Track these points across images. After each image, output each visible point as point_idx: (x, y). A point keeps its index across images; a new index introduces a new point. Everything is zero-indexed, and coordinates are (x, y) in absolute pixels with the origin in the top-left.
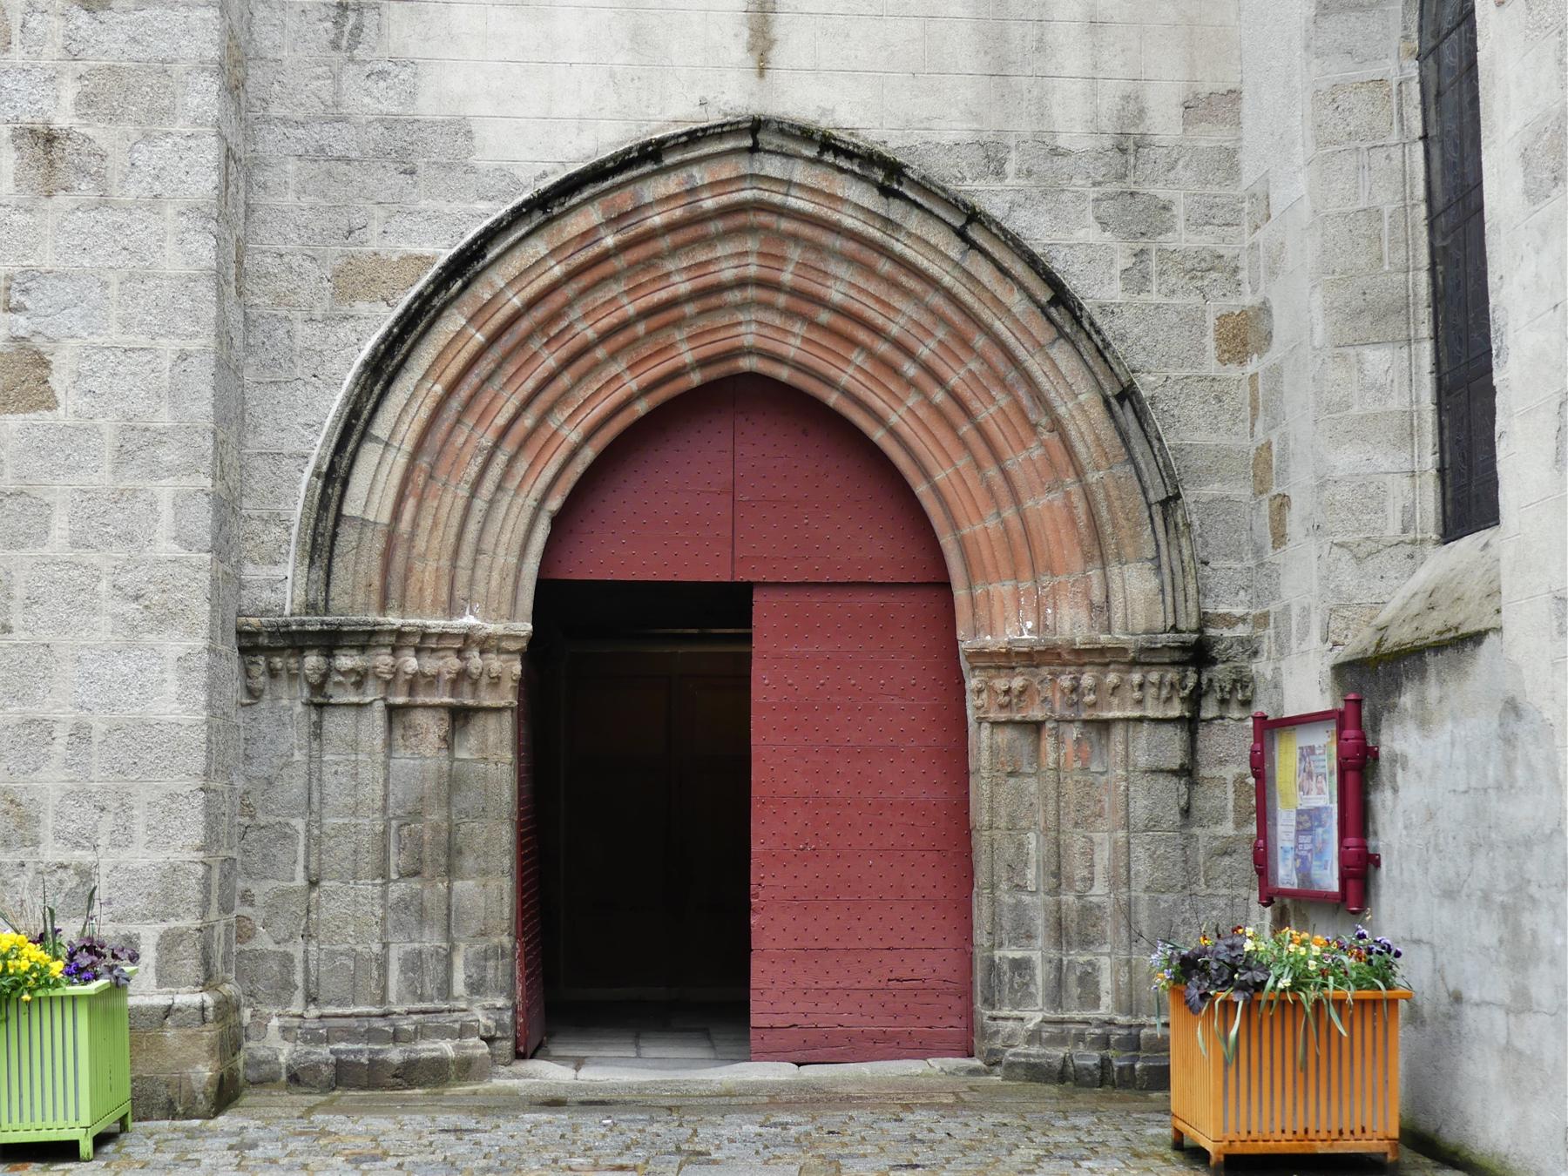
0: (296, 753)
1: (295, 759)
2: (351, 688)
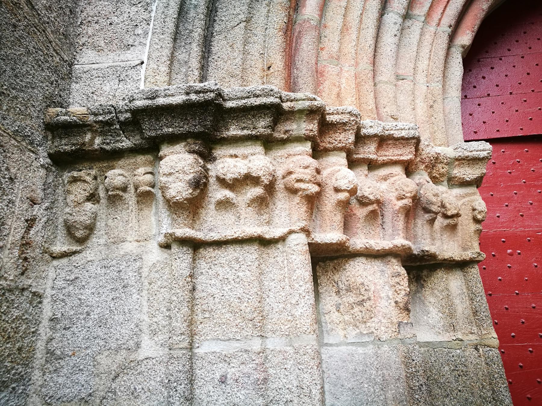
0: (146, 341)
1: (142, 354)
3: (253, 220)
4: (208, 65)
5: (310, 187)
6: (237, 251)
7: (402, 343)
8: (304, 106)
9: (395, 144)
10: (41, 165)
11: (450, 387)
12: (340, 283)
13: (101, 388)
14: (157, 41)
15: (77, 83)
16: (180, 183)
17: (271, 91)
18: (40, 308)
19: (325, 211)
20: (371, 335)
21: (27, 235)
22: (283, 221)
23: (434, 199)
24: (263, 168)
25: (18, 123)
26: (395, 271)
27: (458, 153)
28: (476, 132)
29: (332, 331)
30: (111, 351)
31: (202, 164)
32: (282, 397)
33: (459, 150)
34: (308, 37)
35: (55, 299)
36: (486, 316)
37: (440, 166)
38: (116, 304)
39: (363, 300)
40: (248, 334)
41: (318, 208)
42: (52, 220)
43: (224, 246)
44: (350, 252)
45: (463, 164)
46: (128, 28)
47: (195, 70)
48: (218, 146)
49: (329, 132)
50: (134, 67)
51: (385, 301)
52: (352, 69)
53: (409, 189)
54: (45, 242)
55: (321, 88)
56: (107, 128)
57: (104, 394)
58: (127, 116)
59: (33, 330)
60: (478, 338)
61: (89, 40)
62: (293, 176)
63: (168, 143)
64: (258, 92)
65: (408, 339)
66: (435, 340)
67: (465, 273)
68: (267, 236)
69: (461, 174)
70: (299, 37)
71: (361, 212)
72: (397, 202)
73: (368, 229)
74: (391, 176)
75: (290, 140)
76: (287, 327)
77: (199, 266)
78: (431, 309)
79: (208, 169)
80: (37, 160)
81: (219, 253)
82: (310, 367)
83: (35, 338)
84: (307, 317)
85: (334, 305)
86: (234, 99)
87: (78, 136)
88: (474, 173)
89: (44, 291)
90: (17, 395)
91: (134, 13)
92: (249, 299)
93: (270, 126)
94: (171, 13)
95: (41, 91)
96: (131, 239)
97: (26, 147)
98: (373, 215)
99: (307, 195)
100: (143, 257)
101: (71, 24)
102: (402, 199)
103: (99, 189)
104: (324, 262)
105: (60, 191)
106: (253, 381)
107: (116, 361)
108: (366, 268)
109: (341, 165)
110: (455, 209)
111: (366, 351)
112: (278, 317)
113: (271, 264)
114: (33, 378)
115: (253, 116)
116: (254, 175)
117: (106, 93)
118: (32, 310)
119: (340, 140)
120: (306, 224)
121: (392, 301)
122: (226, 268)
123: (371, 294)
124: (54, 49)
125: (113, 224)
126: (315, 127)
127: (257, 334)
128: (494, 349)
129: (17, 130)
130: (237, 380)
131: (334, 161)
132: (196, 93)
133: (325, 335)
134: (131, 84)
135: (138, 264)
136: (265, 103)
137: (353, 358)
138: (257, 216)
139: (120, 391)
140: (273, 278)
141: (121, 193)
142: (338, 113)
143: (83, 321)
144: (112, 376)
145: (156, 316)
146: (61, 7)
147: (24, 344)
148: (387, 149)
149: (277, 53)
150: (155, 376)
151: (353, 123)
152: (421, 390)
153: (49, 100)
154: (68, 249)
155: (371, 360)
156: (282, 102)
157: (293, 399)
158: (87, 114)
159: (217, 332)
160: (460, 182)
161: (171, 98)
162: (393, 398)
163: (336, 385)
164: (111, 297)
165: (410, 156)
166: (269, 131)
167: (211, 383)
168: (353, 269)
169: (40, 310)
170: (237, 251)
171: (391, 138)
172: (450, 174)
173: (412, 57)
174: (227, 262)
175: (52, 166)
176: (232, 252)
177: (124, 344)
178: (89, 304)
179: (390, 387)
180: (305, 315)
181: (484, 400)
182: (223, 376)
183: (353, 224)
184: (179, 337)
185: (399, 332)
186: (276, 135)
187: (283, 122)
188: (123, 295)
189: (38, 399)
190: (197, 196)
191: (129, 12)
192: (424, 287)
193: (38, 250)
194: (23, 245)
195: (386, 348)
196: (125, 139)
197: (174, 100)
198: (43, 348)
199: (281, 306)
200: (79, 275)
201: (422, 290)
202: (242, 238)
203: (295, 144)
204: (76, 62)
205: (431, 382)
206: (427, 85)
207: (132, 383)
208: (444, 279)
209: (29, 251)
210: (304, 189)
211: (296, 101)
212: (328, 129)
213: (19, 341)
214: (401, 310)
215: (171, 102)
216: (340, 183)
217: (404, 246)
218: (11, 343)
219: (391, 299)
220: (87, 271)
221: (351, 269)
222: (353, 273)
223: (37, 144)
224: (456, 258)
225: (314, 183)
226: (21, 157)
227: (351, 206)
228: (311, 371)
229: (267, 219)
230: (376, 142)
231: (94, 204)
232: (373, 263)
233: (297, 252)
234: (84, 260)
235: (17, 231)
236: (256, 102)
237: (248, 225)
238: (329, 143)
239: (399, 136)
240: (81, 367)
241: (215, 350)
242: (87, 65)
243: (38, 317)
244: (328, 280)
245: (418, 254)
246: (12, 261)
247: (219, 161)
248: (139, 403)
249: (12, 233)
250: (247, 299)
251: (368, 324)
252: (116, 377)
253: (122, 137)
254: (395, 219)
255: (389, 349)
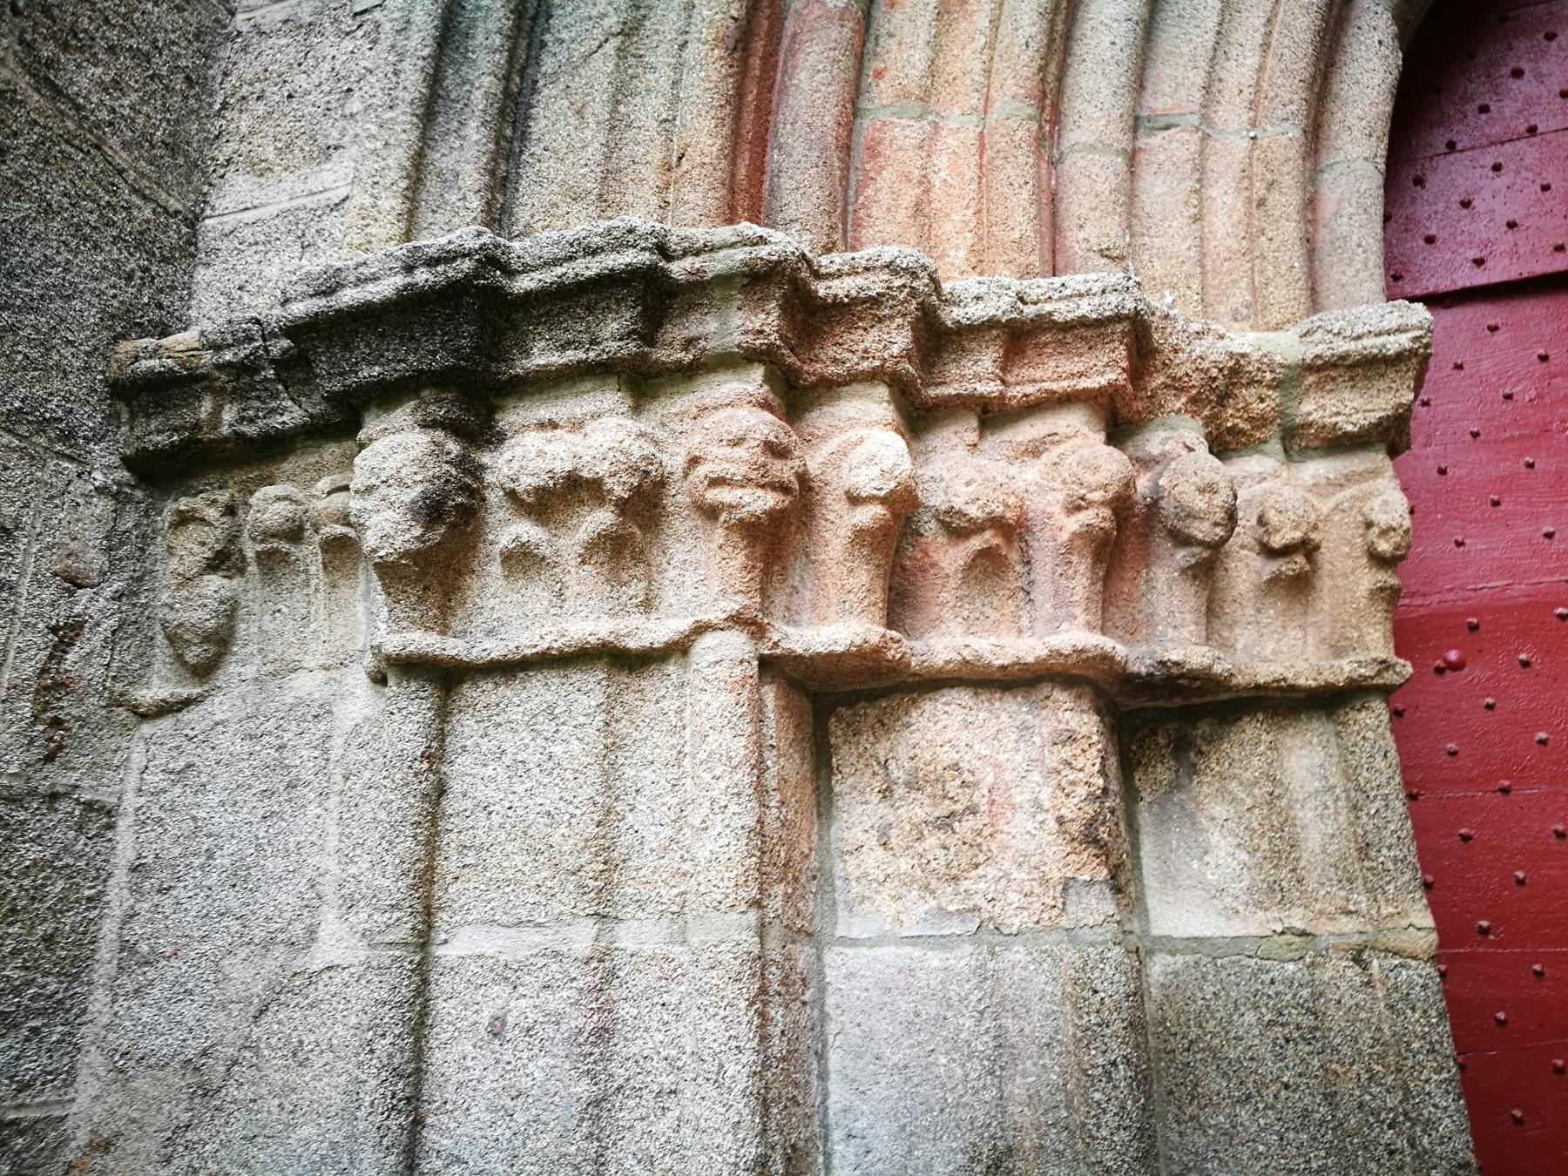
0: (331, 925)
1: (318, 958)
2: (583, 580)
3: (596, 601)
4: (518, 174)
5: (747, 499)
6: (553, 688)
7: (1070, 941)
8: (731, 264)
9: (1062, 344)
10: (97, 489)
11: (1256, 1073)
12: (892, 765)
13: (229, 1037)
14: (374, 129)
15: (207, 265)
16: (390, 514)
17: (631, 231)
18: (110, 840)
19: (824, 561)
20: (970, 915)
21: (59, 663)
22: (690, 597)
23: (1199, 503)
24: (611, 454)
25: (22, 391)
26: (1062, 726)
27: (1311, 346)
28: (1479, 262)
29: (862, 902)
30: (252, 947)
31: (453, 456)
32: (649, 1079)
33: (1318, 336)
34: (816, 49)
35: (143, 817)
36: (1395, 860)
37: (1250, 394)
38: (271, 831)
39: (952, 814)
40: (563, 908)
41: (807, 555)
42: (135, 622)
43: (521, 675)
44: (915, 674)
45: (1334, 379)
46: (329, 102)
47: (471, 196)
48: (511, 400)
49: (832, 328)
50: (336, 205)
51: (1025, 816)
52: (970, 122)
53: (1101, 477)
54: (114, 678)
55: (869, 192)
56: (247, 379)
57: (236, 1054)
58: (286, 345)
59: (87, 893)
60: (1369, 928)
61: (244, 148)
62: (702, 470)
63: (379, 406)
64: (596, 241)
65: (1086, 929)
66: (1218, 933)
67: (1340, 728)
68: (632, 644)
69: (1327, 413)
70: (792, 53)
71: (951, 557)
72: (1066, 520)
73: (978, 604)
74: (1053, 443)
75: (705, 364)
76: (675, 891)
77: (460, 729)
78: (1215, 838)
79: (483, 467)
80: (85, 477)
81: (508, 693)
82: (726, 1001)
83: (97, 912)
84: (729, 864)
85: (872, 827)
86: (534, 268)
87: (184, 407)
88: (1370, 407)
89: (119, 799)
90: (45, 1046)
91: (345, 58)
92: (573, 816)
93: (634, 331)
94: (414, 44)
95: (95, 301)
96: (312, 665)
97: (47, 448)
98: (988, 566)
99: (741, 520)
100: (334, 709)
101: (193, 111)
102: (1079, 508)
103: (242, 539)
104: (851, 705)
105: (160, 549)
106: (566, 1035)
107: (262, 971)
108: (970, 719)
109: (870, 425)
110: (1296, 528)
111: (951, 961)
112: (655, 863)
113: (647, 720)
114: (90, 1007)
115: (588, 308)
116: (585, 474)
117: (270, 284)
118: (86, 845)
119: (866, 351)
120: (747, 602)
121: (1049, 816)
122: (524, 734)
123: (980, 797)
124: (133, 187)
125: (272, 626)
126: (769, 321)
127: (587, 911)
128: (1413, 963)
129: (20, 410)
130: (529, 1030)
131: (852, 413)
132: (428, 265)
133: (842, 914)
134: (328, 253)
135: (322, 726)
136: (612, 270)
137: (911, 979)
138: (609, 588)
139: (269, 1046)
140: (650, 758)
141: (284, 546)
142: (854, 272)
143: (198, 873)
144: (252, 1010)
145: (356, 859)
146: (154, 74)
147: (61, 926)
148: (1037, 359)
149: (703, 113)
150: (345, 1013)
151: (901, 297)
152: (1110, 1079)
153: (123, 320)
154: (172, 695)
155: (961, 986)
156: (669, 258)
157: (681, 1087)
158: (197, 349)
159: (493, 904)
160: (1324, 439)
161: (370, 287)
162: (1030, 1097)
163: (860, 1056)
164: (261, 812)
165: (1113, 376)
166: (633, 346)
167: (471, 1035)
168: (931, 724)
169: (109, 845)
170: (553, 688)
171: (1044, 324)
172: (1287, 415)
173: (1200, 51)
174: (527, 718)
175: (133, 487)
176: (540, 691)
177: (282, 930)
178: (214, 829)
179: (1020, 1067)
180: (723, 858)
181: (1371, 1119)
182: (497, 1019)
183: (930, 595)
184: (387, 915)
185: (1063, 910)
186: (662, 355)
187: (680, 316)
188: (286, 806)
189: (101, 1059)
190: (439, 544)
191: (334, 57)
192: (1196, 773)
193: (93, 700)
194: (46, 688)
195: (1018, 953)
196: (290, 403)
197: (374, 290)
198: (113, 936)
199: (668, 832)
200: (196, 759)
201: (1191, 781)
202: (560, 650)
203: (720, 377)
204: (208, 212)
205: (1199, 1056)
206: (1252, 134)
207: (295, 1029)
208: (1262, 748)
209: (65, 704)
210: (731, 506)
211: (711, 250)
212: (830, 322)
213: (45, 920)
214: (1076, 844)
215: (369, 297)
216: (856, 479)
217: (1082, 651)
218: (19, 924)
219: (1047, 811)
220: (213, 748)
221: (923, 722)
222: (929, 737)
223: (85, 438)
224: (1302, 682)
225: (763, 487)
226: (32, 474)
227: (923, 540)
228: (727, 1013)
229: (641, 593)
230: (999, 342)
231: (230, 578)
232: (997, 704)
233: (716, 683)
234: (207, 721)
235: (24, 655)
236: (587, 268)
237: (584, 614)
238: (835, 361)
239: (1070, 316)
240: (190, 986)
241: (484, 950)
242: (232, 216)
243: (104, 861)
244: (860, 756)
245: (1150, 675)
246: (13, 729)
247: (513, 441)
248: (307, 1079)
249: (10, 661)
250: (567, 817)
251: (965, 884)
252: (261, 1012)
253: (284, 399)
254: (1060, 571)
255: (1029, 958)
